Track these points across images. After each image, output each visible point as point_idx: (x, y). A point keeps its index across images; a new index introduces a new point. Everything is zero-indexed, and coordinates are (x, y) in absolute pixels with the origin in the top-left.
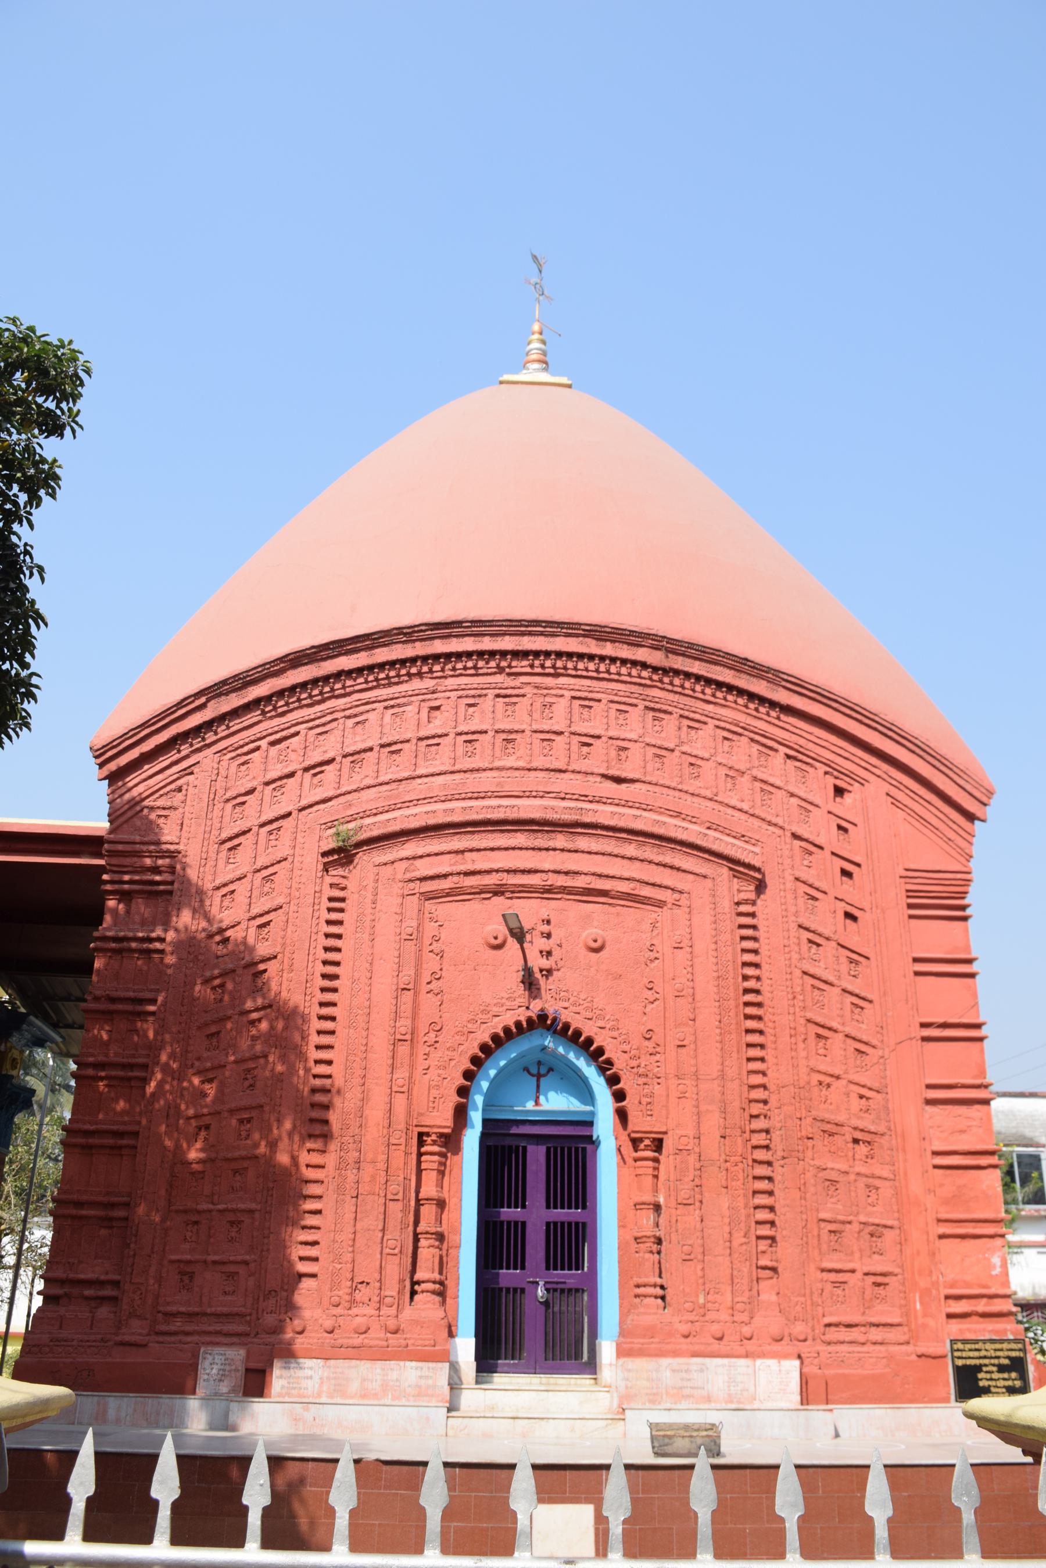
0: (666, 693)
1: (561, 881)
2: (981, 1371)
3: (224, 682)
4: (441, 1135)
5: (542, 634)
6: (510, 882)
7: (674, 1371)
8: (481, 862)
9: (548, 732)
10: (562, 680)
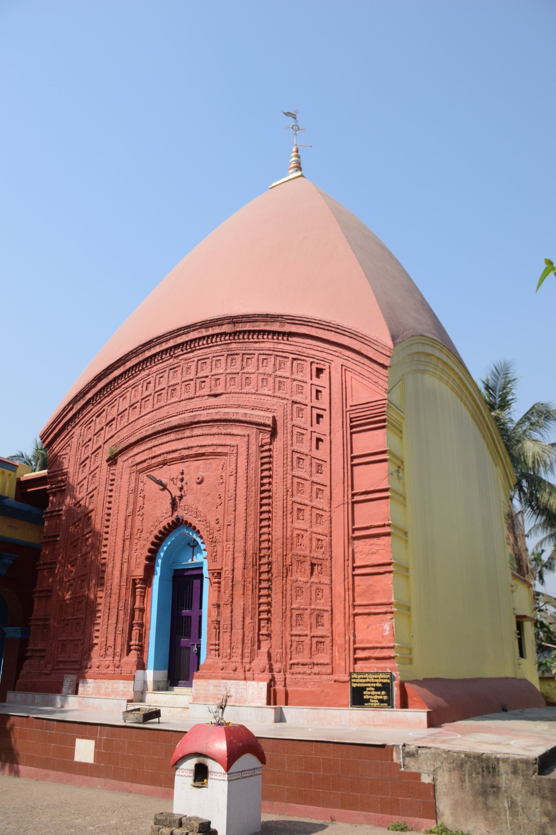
0: (237, 344)
1: (185, 453)
2: (365, 690)
3: (77, 396)
4: (140, 579)
5: (183, 334)
6: (168, 458)
7: (214, 686)
8: (157, 451)
9: (188, 381)
10: (196, 353)
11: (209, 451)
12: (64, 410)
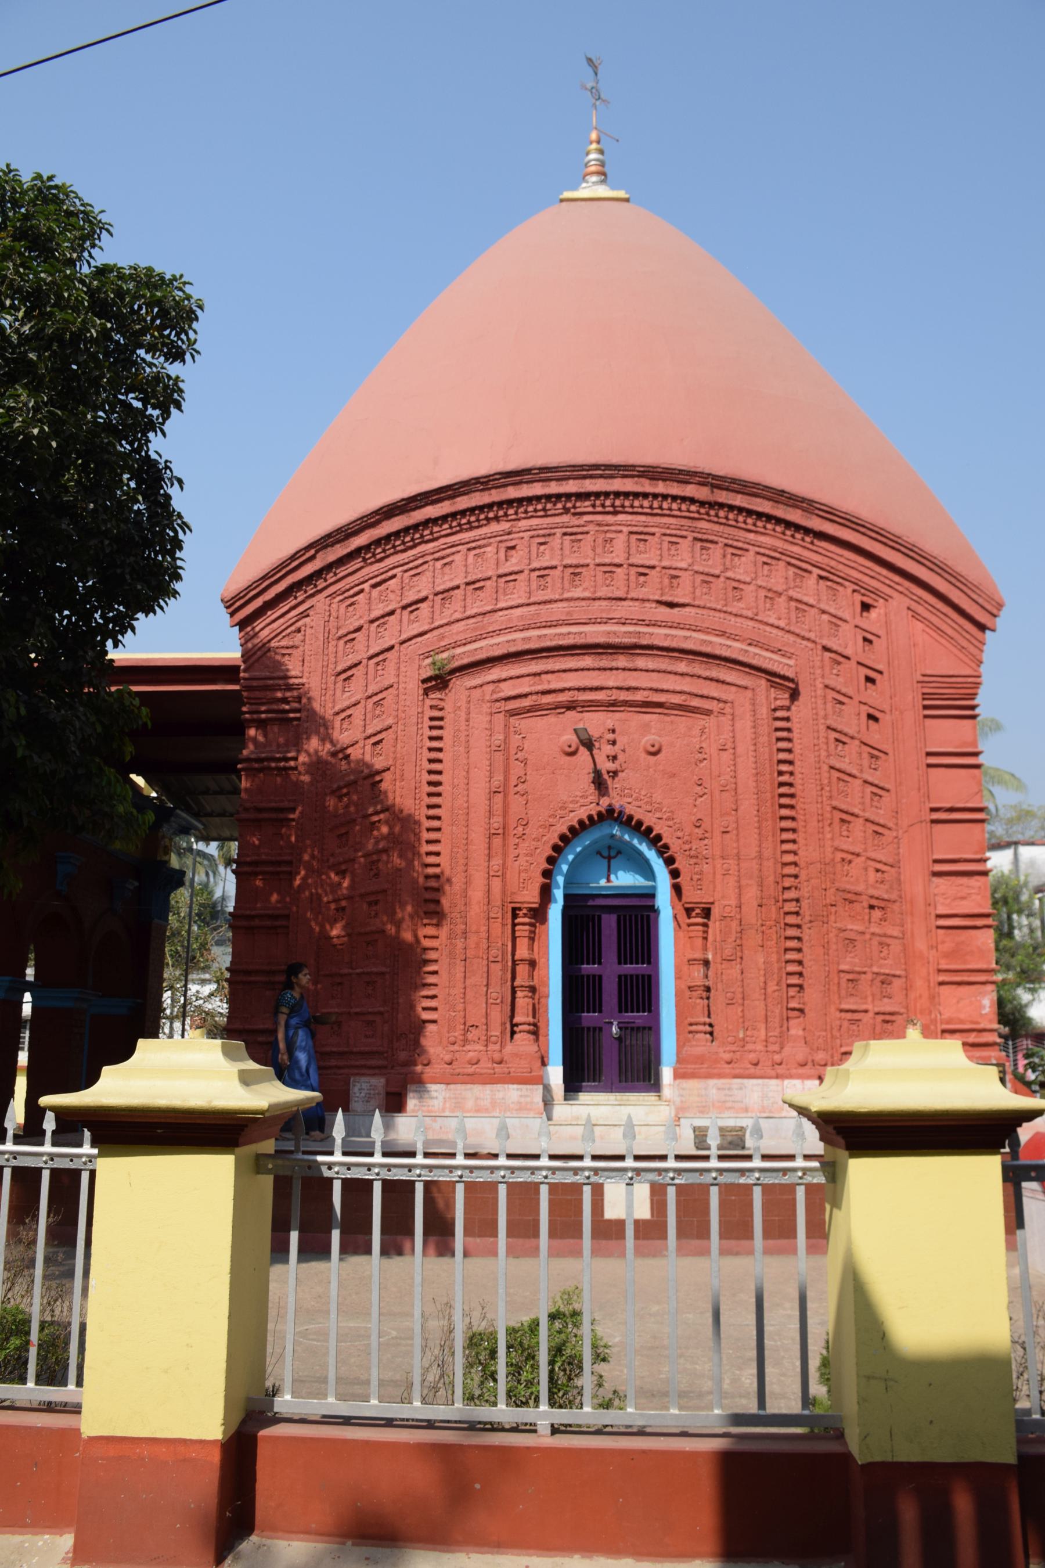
1: (623, 696)
3: (329, 536)
4: (530, 909)
5: (601, 476)
6: (580, 698)
7: (719, 1089)
9: (609, 565)
11: (673, 701)
12: (293, 558)
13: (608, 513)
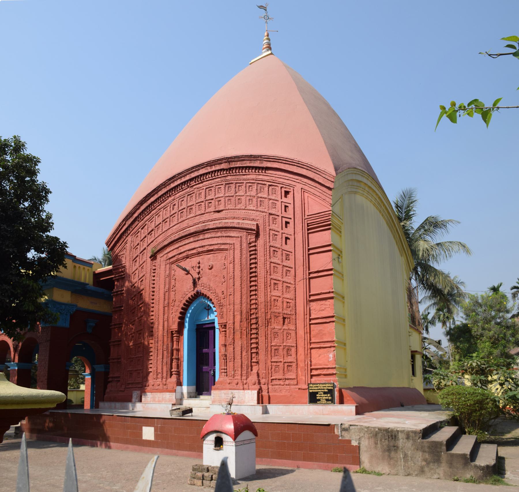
1: (200, 250)
3: (127, 216)
4: (176, 331)
5: (196, 171)
8: (182, 249)
10: (204, 183)
12: (120, 225)
13: (200, 183)
